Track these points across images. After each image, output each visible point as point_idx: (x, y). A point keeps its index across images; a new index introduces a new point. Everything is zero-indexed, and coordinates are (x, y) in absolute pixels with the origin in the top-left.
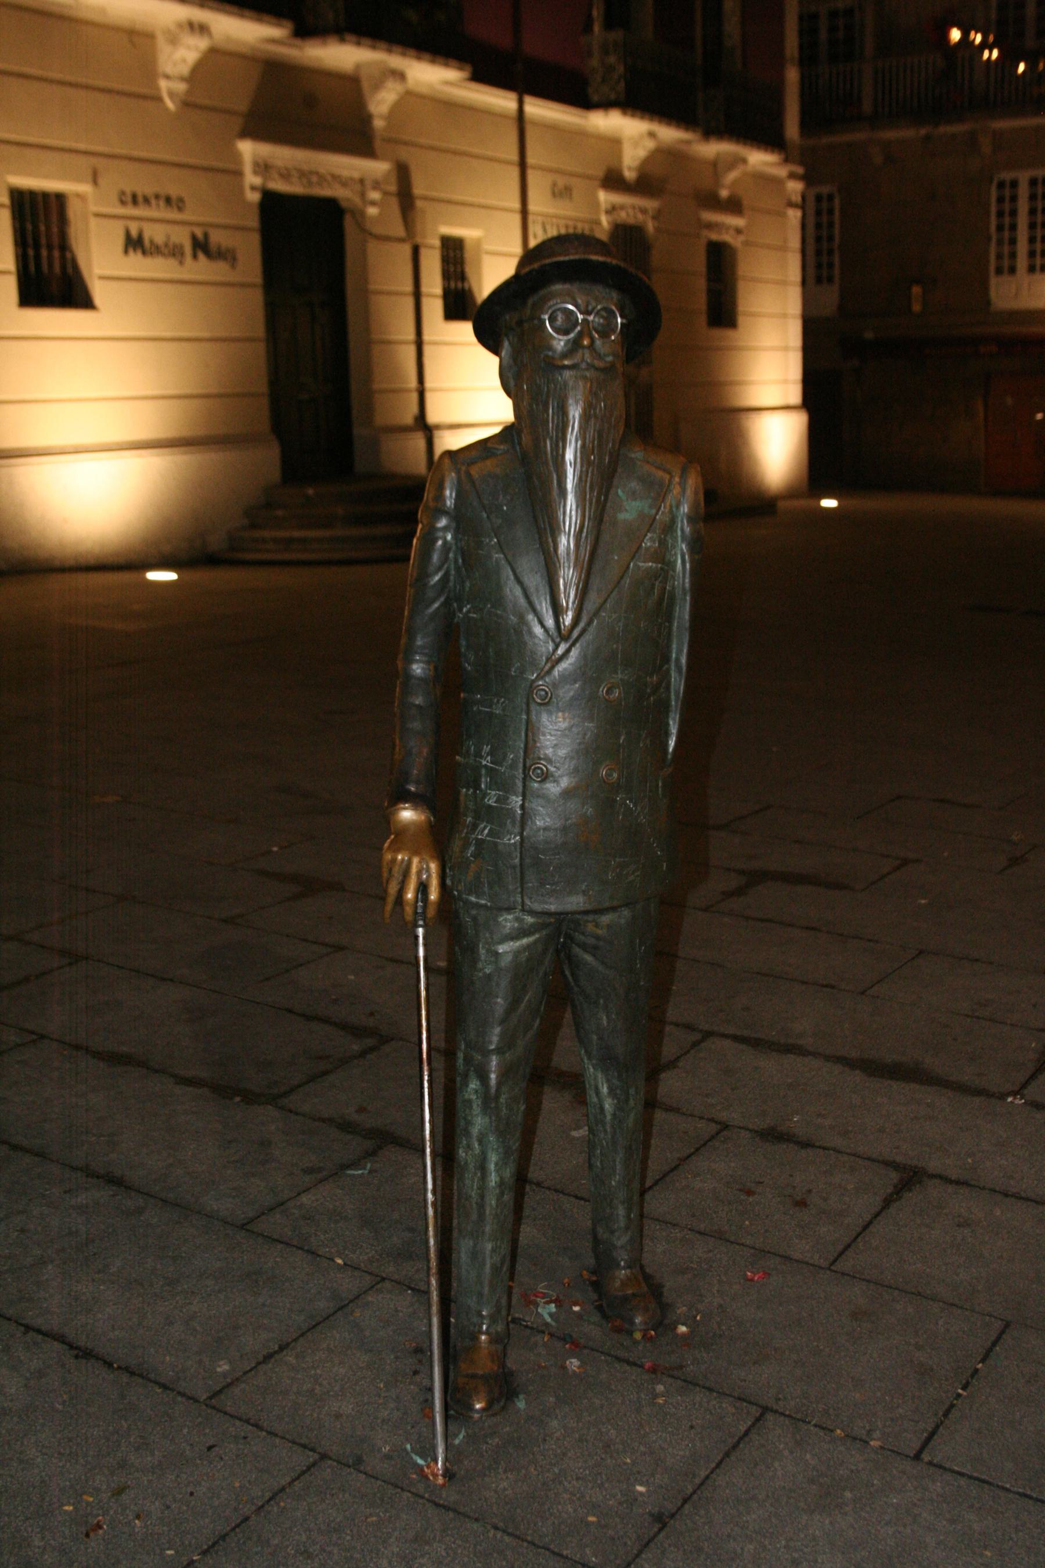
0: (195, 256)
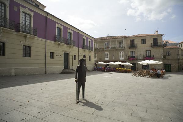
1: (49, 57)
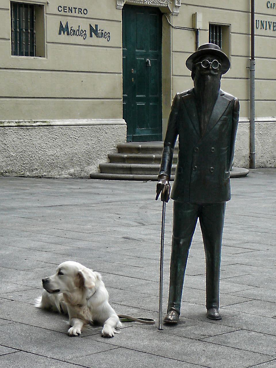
0: (91, 36)
1: (8, 45)
